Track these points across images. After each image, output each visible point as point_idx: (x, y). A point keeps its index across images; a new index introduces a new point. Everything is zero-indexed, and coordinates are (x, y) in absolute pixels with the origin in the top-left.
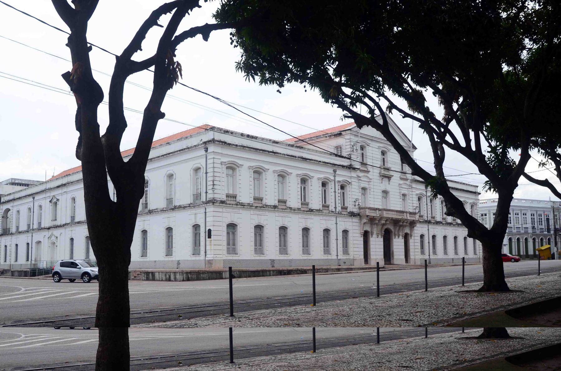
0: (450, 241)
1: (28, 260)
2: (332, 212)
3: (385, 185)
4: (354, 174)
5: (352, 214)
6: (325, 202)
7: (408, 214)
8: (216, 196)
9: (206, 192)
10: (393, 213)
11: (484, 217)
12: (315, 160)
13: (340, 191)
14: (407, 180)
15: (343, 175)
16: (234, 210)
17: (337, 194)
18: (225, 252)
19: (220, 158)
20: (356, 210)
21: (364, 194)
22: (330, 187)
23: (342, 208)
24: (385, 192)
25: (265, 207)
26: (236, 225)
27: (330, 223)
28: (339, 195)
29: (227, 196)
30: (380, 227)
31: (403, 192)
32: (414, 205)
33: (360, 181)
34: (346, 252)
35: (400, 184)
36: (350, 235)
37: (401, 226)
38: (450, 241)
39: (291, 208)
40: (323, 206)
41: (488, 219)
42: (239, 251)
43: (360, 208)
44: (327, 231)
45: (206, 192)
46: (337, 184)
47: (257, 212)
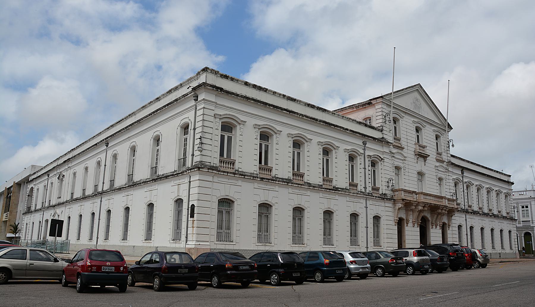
0: (487, 232)
1: (91, 239)
2: (361, 192)
3: (420, 166)
4: (386, 150)
5: (383, 197)
6: (353, 180)
7: (447, 200)
8: (206, 159)
9: (193, 155)
10: (431, 198)
11: (525, 209)
12: (341, 127)
13: (370, 168)
14: (443, 162)
15: (373, 149)
16: (230, 181)
17: (367, 170)
18: (214, 238)
19: (213, 108)
20: (389, 193)
21: (397, 174)
22: (359, 163)
23: (373, 189)
24: (421, 174)
25: (275, 180)
26: (233, 202)
27: (359, 206)
28: (370, 173)
29: (293, 175)
30: (416, 214)
31: (440, 175)
32: (451, 191)
33: (393, 158)
34: (377, 243)
35: (436, 166)
36: (383, 222)
37: (439, 214)
38: (487, 232)
39: (309, 184)
40: (350, 185)
41: (530, 211)
42: (234, 237)
43: (393, 191)
44: (354, 216)
45: (193, 155)
46: (367, 160)
47: (262, 185)
